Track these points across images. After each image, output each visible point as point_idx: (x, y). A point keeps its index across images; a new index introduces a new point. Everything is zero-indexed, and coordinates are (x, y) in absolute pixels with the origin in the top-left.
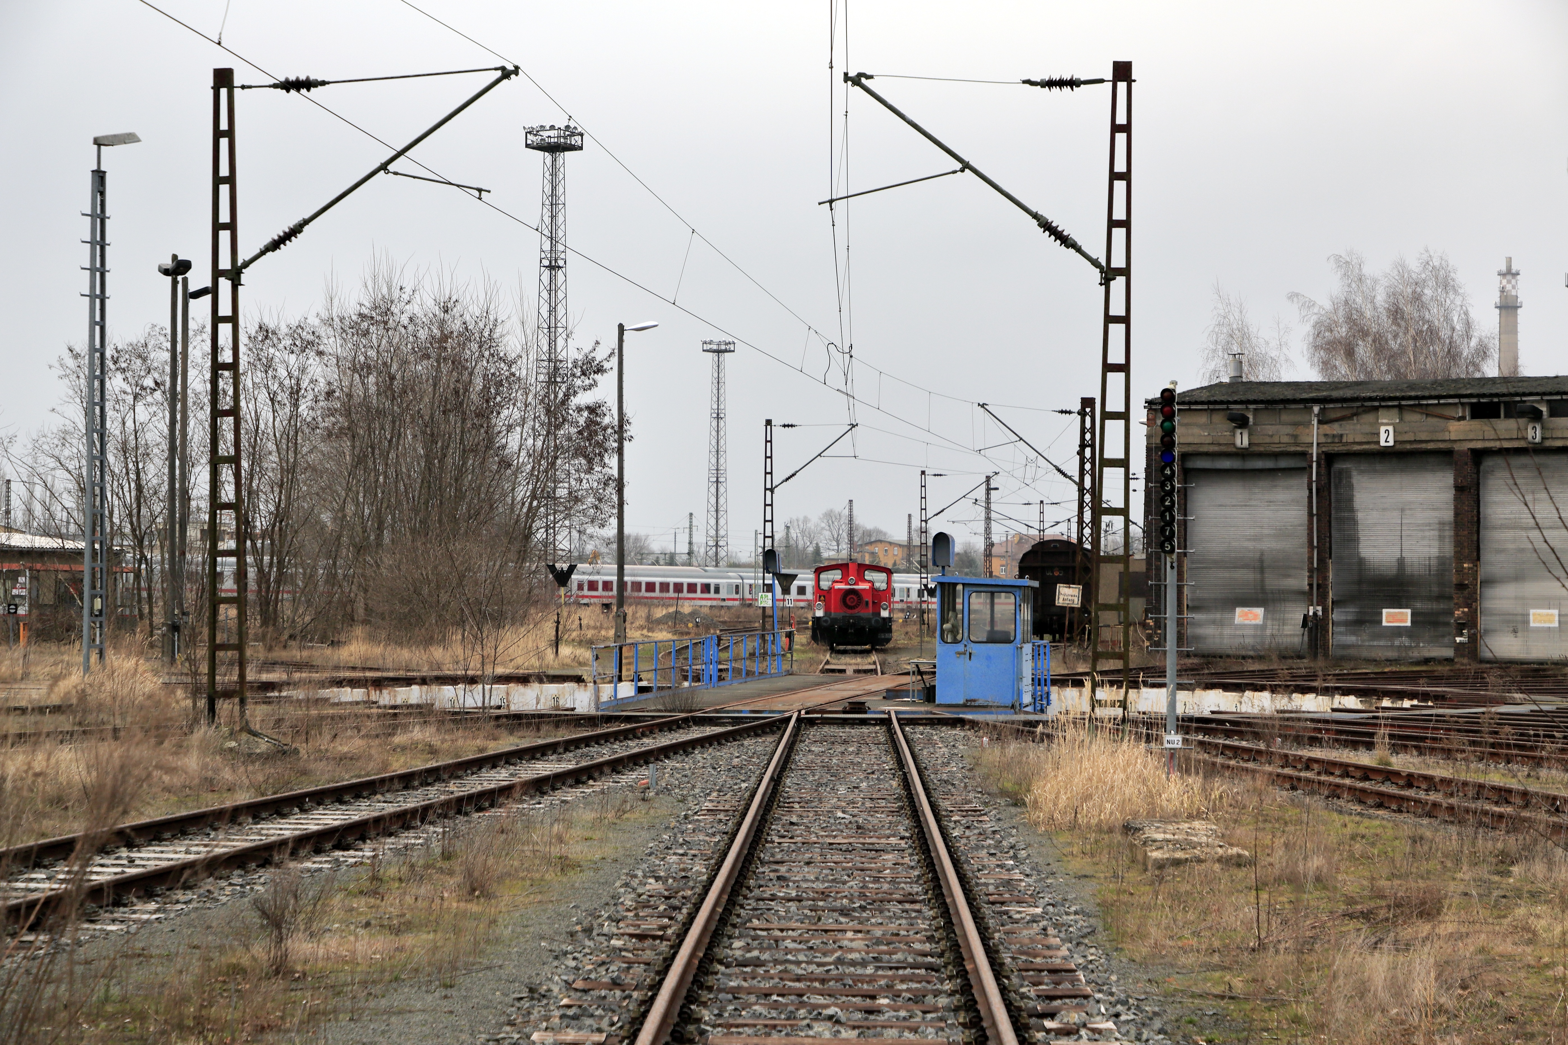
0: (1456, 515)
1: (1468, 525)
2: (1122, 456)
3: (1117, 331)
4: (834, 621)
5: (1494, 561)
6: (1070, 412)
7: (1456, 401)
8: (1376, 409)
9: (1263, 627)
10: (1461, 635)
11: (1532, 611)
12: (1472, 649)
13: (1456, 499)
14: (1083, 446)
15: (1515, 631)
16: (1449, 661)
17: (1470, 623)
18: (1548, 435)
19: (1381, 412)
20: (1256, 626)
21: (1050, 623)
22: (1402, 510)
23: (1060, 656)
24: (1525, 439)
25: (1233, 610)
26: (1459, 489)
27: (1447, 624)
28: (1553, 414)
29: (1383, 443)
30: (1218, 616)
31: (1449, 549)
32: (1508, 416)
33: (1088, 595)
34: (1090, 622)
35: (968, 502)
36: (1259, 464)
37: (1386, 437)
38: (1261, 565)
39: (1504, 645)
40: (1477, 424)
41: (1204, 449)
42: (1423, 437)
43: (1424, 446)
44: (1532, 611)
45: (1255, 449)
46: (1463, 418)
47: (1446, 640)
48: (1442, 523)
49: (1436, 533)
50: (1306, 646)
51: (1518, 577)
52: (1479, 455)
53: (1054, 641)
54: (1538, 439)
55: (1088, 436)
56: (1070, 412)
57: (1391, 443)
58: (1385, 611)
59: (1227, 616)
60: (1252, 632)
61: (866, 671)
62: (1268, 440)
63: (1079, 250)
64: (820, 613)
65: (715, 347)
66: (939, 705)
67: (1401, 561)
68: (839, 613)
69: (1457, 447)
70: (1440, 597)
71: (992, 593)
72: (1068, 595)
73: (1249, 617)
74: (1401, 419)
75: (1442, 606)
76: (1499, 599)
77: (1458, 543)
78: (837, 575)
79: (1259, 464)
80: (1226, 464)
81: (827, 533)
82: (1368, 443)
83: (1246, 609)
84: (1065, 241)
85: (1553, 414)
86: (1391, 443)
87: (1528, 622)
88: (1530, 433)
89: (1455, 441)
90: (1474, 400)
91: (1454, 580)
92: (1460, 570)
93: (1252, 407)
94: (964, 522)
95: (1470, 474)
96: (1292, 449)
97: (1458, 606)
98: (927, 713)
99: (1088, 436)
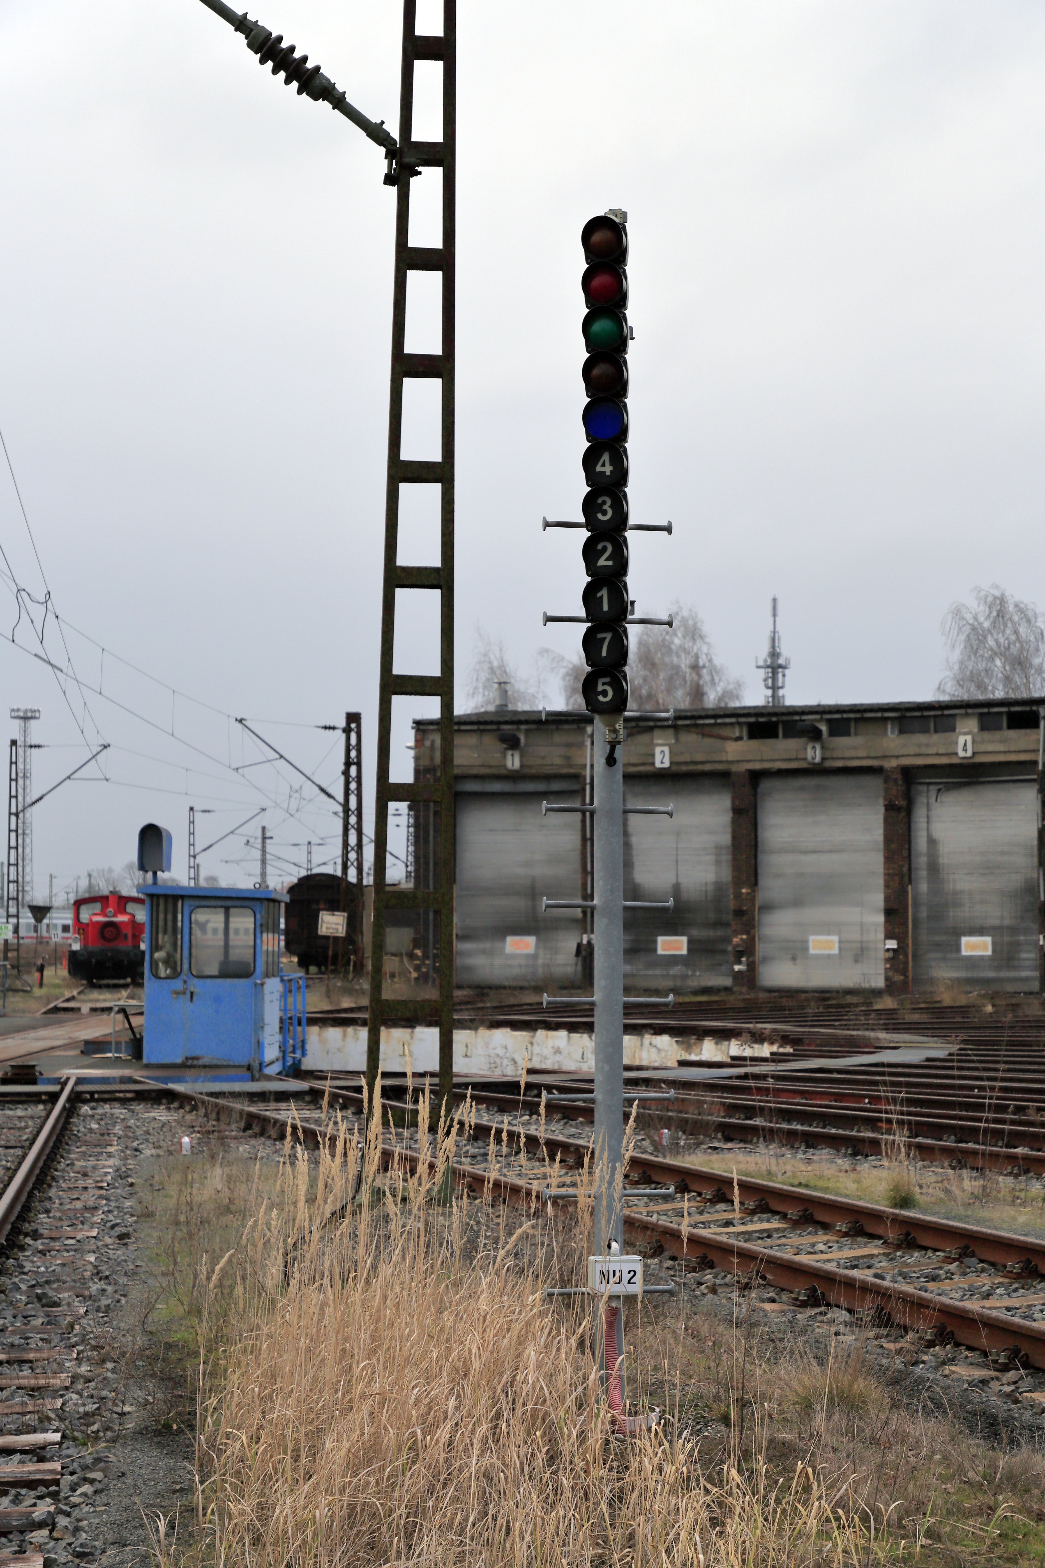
0: (734, 838)
1: (746, 849)
2: (435, 561)
3: (425, 284)
4: (91, 954)
5: (772, 886)
6: (334, 728)
7: (733, 720)
8: (651, 729)
9: (535, 957)
10: (740, 963)
11: (812, 938)
12: (750, 978)
13: (734, 822)
14: (348, 764)
15: (794, 959)
16: (727, 989)
17: (747, 951)
18: (828, 755)
19: (656, 732)
20: (528, 956)
21: (315, 954)
22: (678, 834)
23: (324, 989)
24: (505, 766)
25: (504, 939)
26: (737, 811)
27: (724, 952)
28: (832, 733)
29: (658, 765)
30: (487, 945)
31: (726, 874)
32: (786, 736)
33: (354, 924)
34: (355, 952)
35: (237, 841)
36: (530, 787)
37: (662, 759)
38: (532, 892)
39: (780, 974)
40: (754, 743)
41: (475, 771)
42: (699, 757)
43: (700, 767)
44: (812, 938)
45: (527, 771)
46: (739, 738)
47: (724, 968)
48: (719, 848)
49: (713, 858)
50: (580, 976)
51: (797, 903)
52: (756, 777)
53: (320, 972)
54: (818, 760)
55: (353, 754)
56: (334, 728)
57: (667, 764)
58: (660, 939)
59: (498, 945)
60: (523, 962)
61: (103, 1010)
62: (539, 762)
63: (339, 102)
64: (76, 947)
65: (22, 714)
66: (147, 1066)
67: (677, 890)
68: (96, 946)
69: (734, 768)
70: (719, 924)
71: (227, 909)
72: (332, 923)
73: (520, 946)
74: (677, 740)
75: (720, 933)
76: (777, 926)
77: (736, 867)
78: (98, 907)
79: (530, 787)
80: (497, 787)
81: (129, 882)
82: (643, 764)
83: (517, 938)
84: (311, 83)
85: (832, 733)
86: (667, 764)
87: (807, 949)
88: (810, 753)
89: (732, 762)
90: (752, 720)
91: (732, 905)
92: (738, 895)
93: (523, 727)
94: (237, 862)
95: (747, 794)
96: (565, 771)
97: (736, 933)
98: (124, 1080)
99: (353, 754)
